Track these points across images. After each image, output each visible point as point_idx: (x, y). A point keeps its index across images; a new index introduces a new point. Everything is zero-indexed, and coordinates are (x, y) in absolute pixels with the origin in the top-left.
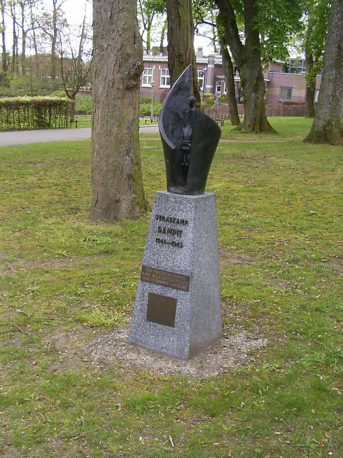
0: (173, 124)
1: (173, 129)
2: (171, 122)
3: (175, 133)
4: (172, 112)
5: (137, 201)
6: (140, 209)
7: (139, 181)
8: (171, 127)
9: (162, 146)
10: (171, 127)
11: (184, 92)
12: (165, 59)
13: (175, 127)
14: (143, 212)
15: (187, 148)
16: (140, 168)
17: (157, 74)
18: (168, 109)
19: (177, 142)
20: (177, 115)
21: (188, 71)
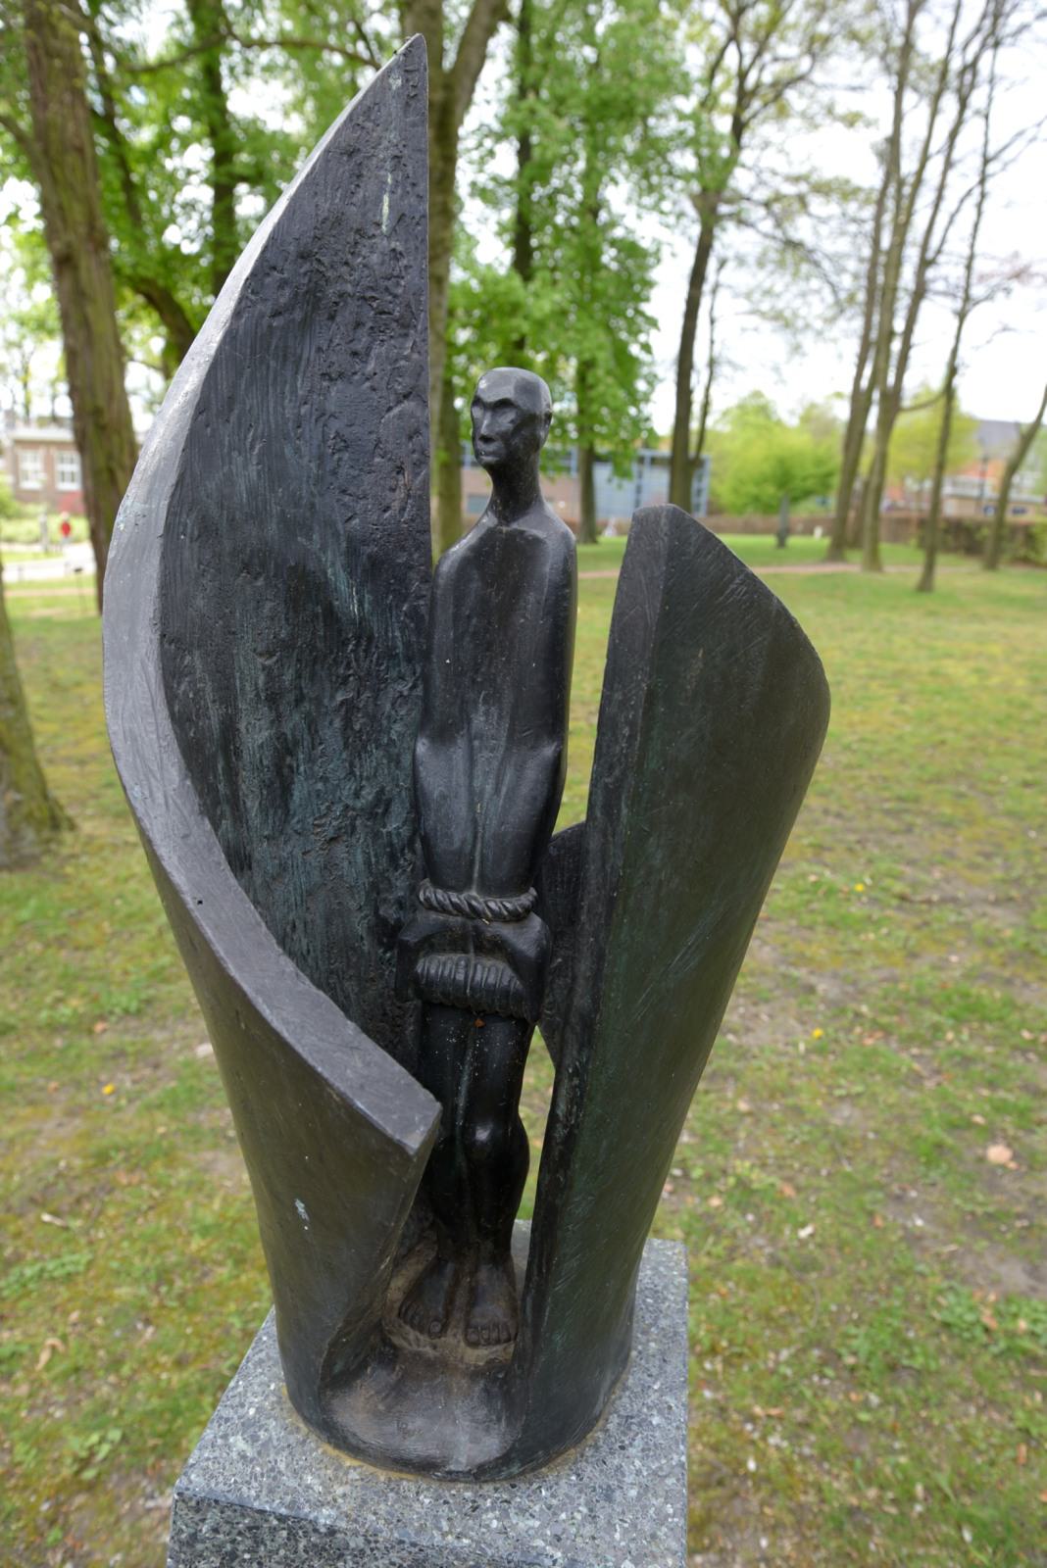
0: (273, 699)
1: (284, 749)
2: (251, 670)
3: (298, 793)
4: (253, 563)
5: (25, 809)
6: (38, 831)
7: (24, 751)
8: (256, 734)
9: (228, 1179)
10: (256, 734)
11: (363, 340)
12: (65, 435)
13: (293, 722)
14: (48, 841)
15: (492, 973)
16: (22, 712)
17: (49, 465)
18: (207, 530)
19: (328, 866)
20: (303, 590)
21: (394, 107)
